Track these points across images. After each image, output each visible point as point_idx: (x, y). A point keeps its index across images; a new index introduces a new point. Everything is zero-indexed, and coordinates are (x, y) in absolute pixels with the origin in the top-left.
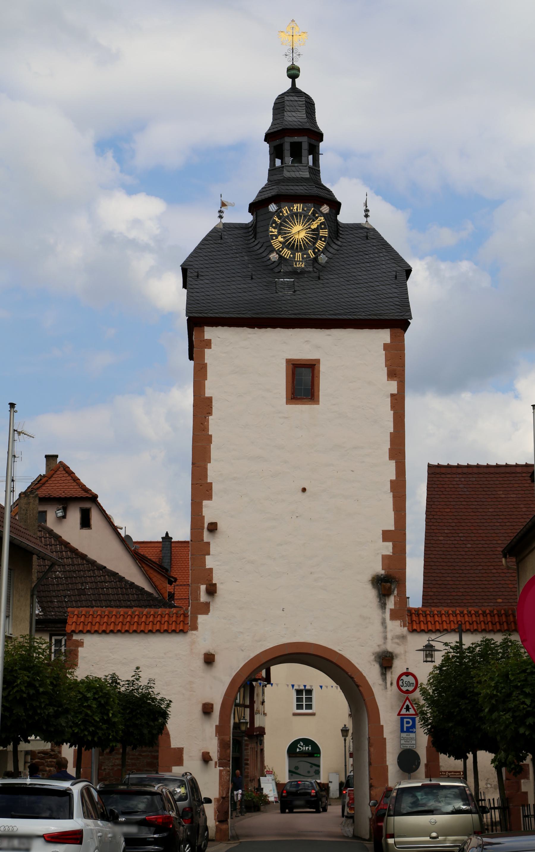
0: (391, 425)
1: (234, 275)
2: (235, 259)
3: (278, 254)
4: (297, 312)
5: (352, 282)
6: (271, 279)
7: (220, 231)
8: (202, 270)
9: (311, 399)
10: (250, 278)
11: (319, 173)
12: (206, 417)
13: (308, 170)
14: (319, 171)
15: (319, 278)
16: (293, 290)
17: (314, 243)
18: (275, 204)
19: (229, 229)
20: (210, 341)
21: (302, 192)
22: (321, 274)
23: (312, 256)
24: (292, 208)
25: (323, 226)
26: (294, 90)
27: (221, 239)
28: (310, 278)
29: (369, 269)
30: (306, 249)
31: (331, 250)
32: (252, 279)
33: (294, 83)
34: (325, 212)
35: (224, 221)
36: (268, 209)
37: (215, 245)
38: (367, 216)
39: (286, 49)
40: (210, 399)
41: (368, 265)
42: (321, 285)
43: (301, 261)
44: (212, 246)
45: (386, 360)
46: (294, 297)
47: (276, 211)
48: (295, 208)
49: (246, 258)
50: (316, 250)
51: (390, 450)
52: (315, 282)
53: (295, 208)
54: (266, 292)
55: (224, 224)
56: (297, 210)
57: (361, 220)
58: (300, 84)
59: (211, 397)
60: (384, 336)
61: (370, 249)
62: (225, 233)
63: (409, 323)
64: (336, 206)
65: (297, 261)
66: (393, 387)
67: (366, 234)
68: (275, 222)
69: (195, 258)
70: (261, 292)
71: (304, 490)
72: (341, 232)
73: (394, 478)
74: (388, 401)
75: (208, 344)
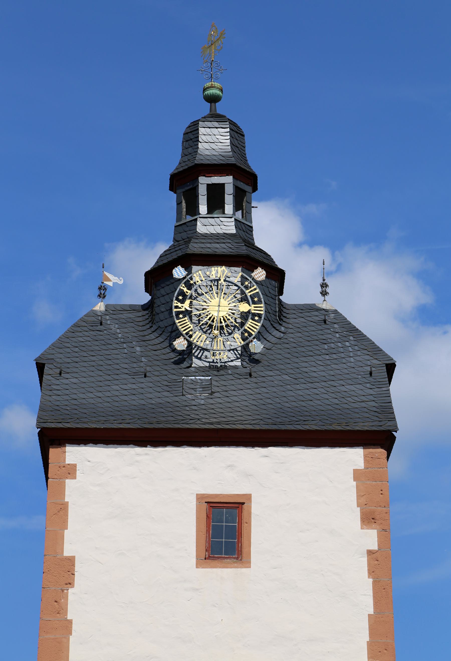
0: (370, 601)
1: (118, 372)
2: (121, 350)
3: (187, 340)
4: (215, 420)
5: (302, 381)
6: (175, 377)
7: (99, 314)
8: (68, 365)
9: (237, 558)
10: (143, 376)
12: (63, 591)
13: (233, 223)
15: (250, 375)
16: (210, 392)
17: (242, 324)
18: (182, 267)
19: (115, 312)
20: (74, 467)
21: (224, 250)
22: (253, 370)
27: (101, 324)
28: (236, 376)
29: (329, 362)
31: (270, 338)
32: (145, 376)
34: (259, 279)
36: (172, 275)
37: (91, 332)
38: (324, 294)
41: (327, 357)
42: (254, 385)
44: (86, 334)
45: (359, 496)
46: (211, 401)
47: (184, 278)
49: (138, 349)
50: (246, 334)
51: (370, 645)
52: (244, 380)
54: (166, 394)
57: (316, 299)
59: (74, 557)
61: (330, 336)
62: (108, 317)
63: (394, 438)
64: (277, 275)
67: (323, 317)
68: (182, 293)
69: (58, 350)
70: (159, 395)
72: (285, 315)
74: (363, 562)
75: (71, 471)
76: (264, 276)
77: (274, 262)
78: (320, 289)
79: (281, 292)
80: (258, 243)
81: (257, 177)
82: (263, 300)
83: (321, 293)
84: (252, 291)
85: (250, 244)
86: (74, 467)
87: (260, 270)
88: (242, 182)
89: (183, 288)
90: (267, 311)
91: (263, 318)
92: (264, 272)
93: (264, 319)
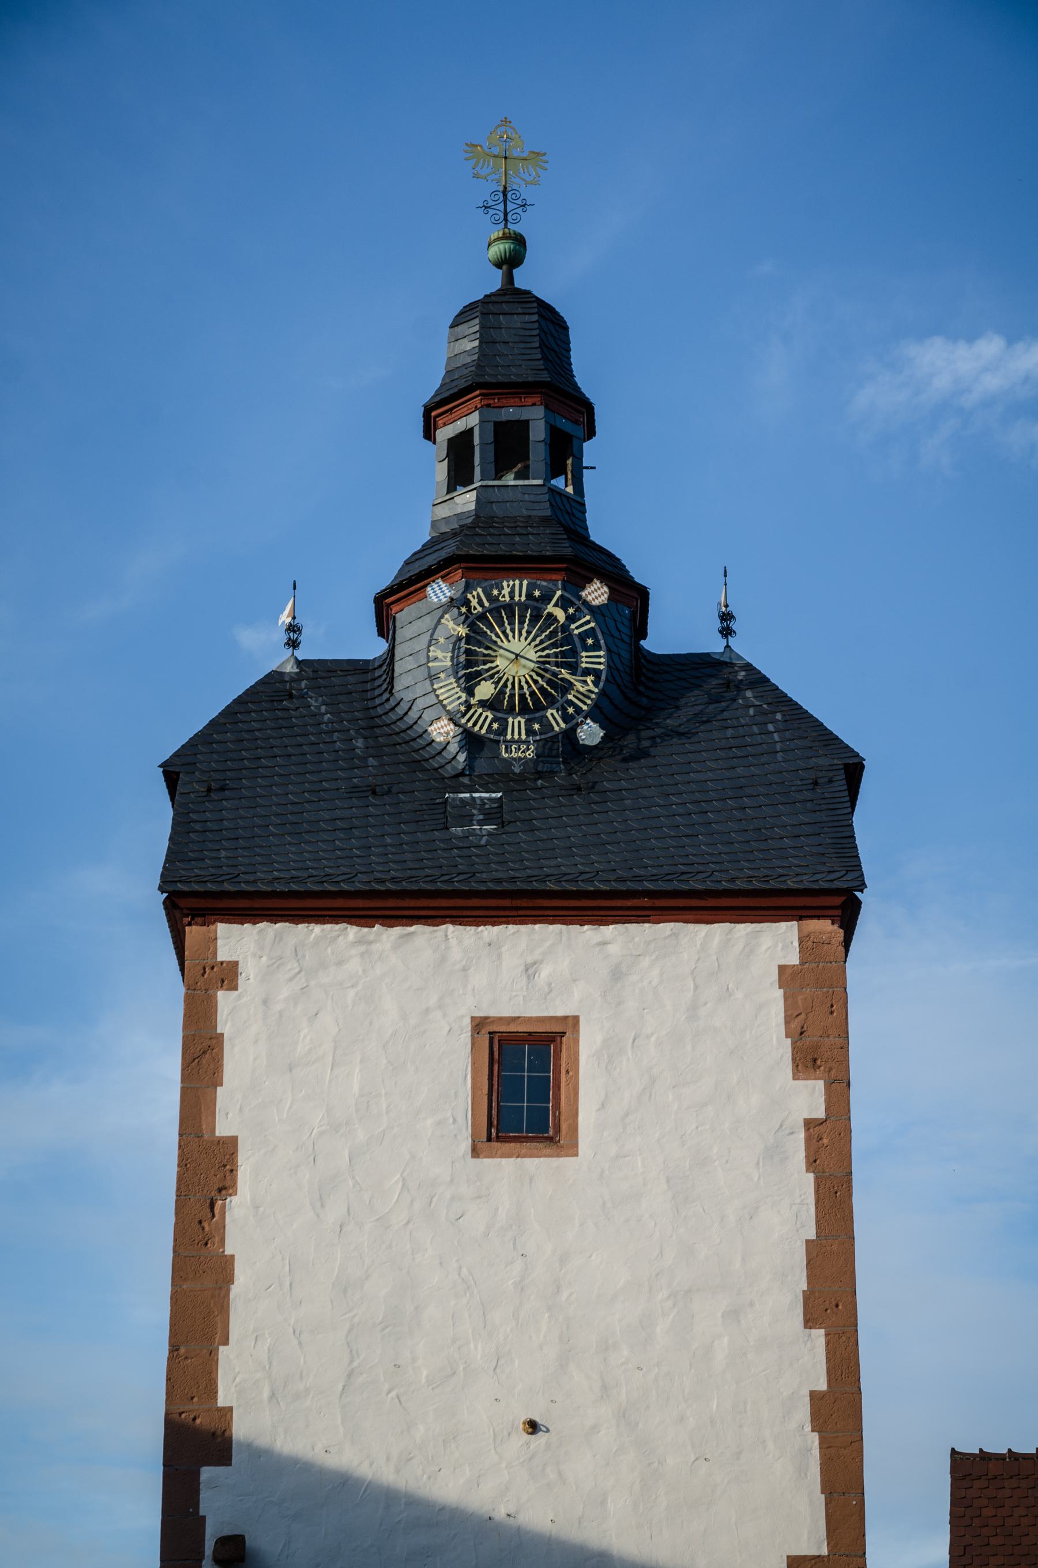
11: (584, 512)
14: (584, 505)
20: (232, 969)
23: (559, 725)
24: (495, 592)
25: (590, 641)
26: (511, 296)
30: (539, 707)
33: (509, 278)
34: (596, 603)
35: (301, 654)
38: (727, 632)
39: (487, 190)
40: (230, 1146)
43: (524, 742)
48: (506, 591)
50: (571, 710)
53: (506, 591)
55: (299, 663)
56: (512, 597)
57: (715, 645)
58: (522, 279)
60: (778, 942)
63: (858, 904)
64: (632, 599)
65: (513, 741)
66: (810, 1098)
71: (533, 1427)
73: (822, 1386)
75: (228, 976)
76: (606, 596)
77: (628, 572)
78: (718, 624)
79: (641, 632)
80: (596, 535)
81: (593, 408)
82: (602, 642)
83: (720, 632)
84: (582, 625)
85: (578, 534)
86: (232, 969)
87: (597, 584)
88: (565, 418)
89: (471, 599)
90: (610, 678)
91: (603, 678)
92: (606, 589)
93: (607, 679)
